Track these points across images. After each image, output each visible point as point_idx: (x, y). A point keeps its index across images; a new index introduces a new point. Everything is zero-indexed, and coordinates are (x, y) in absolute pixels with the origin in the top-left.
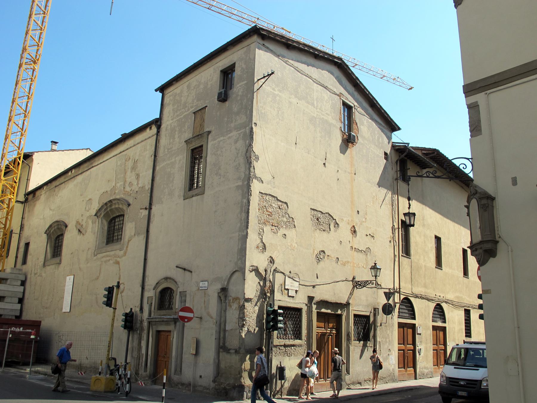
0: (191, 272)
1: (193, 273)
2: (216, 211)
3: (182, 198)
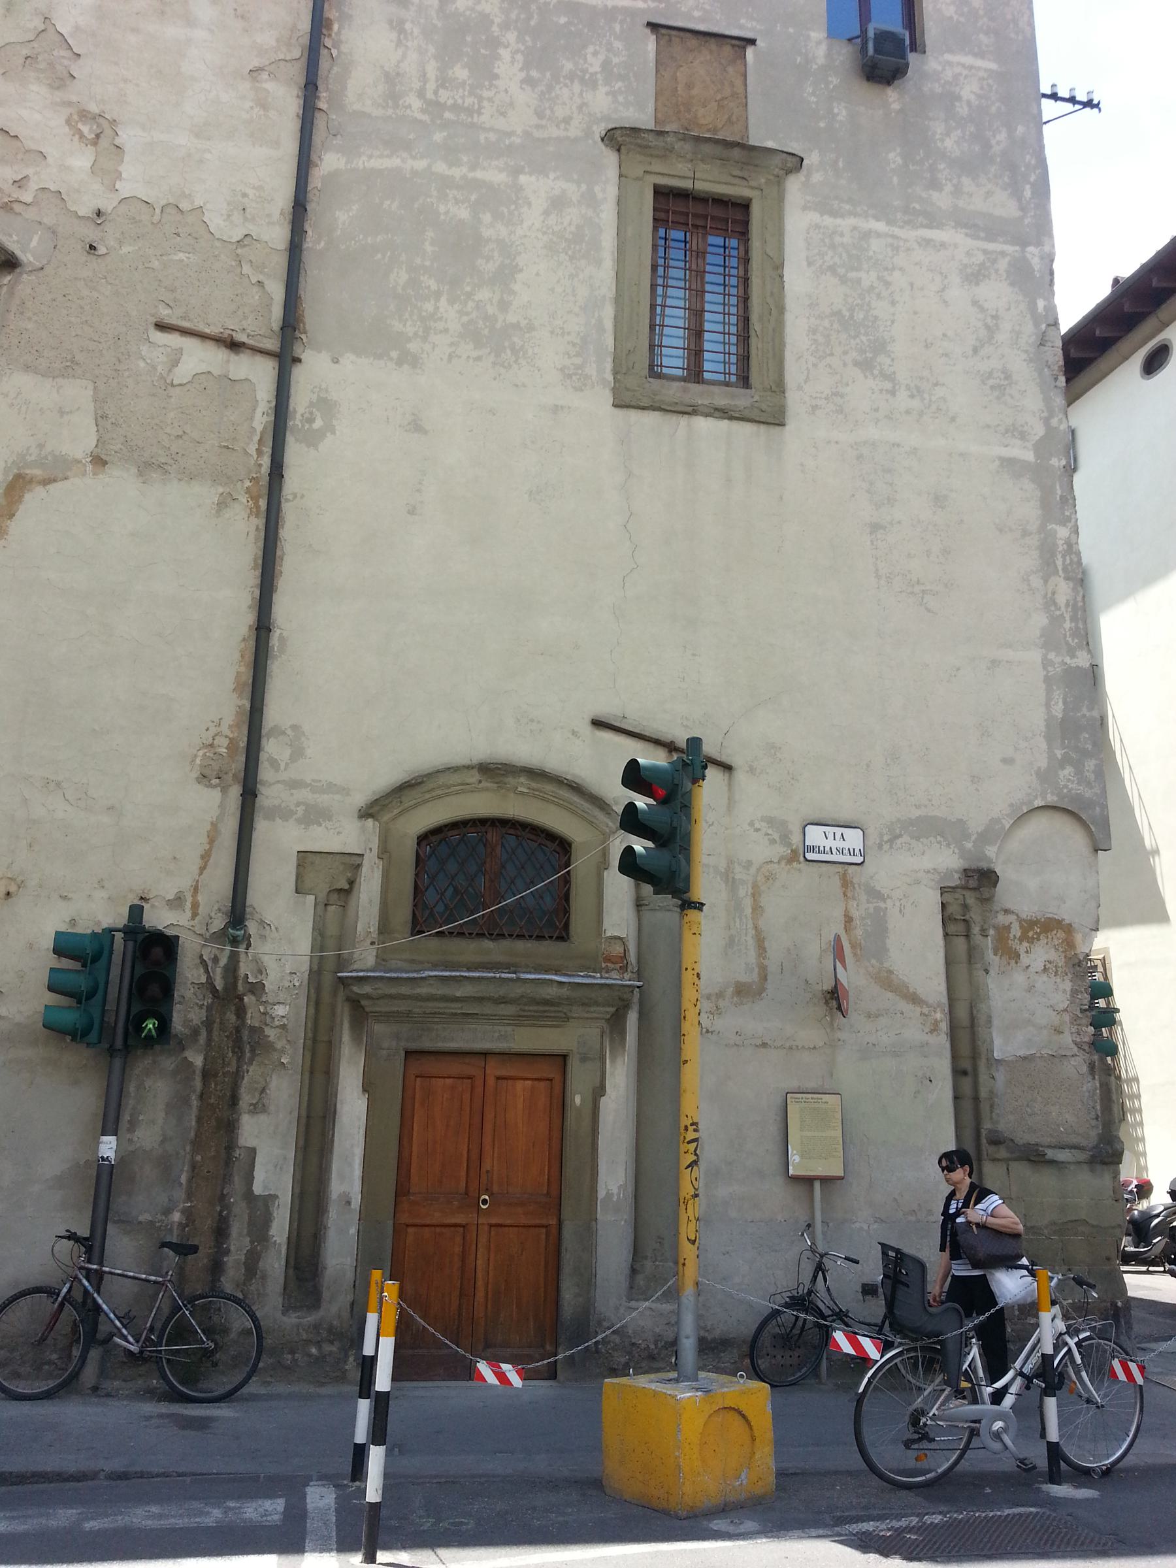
1: (740, 776)
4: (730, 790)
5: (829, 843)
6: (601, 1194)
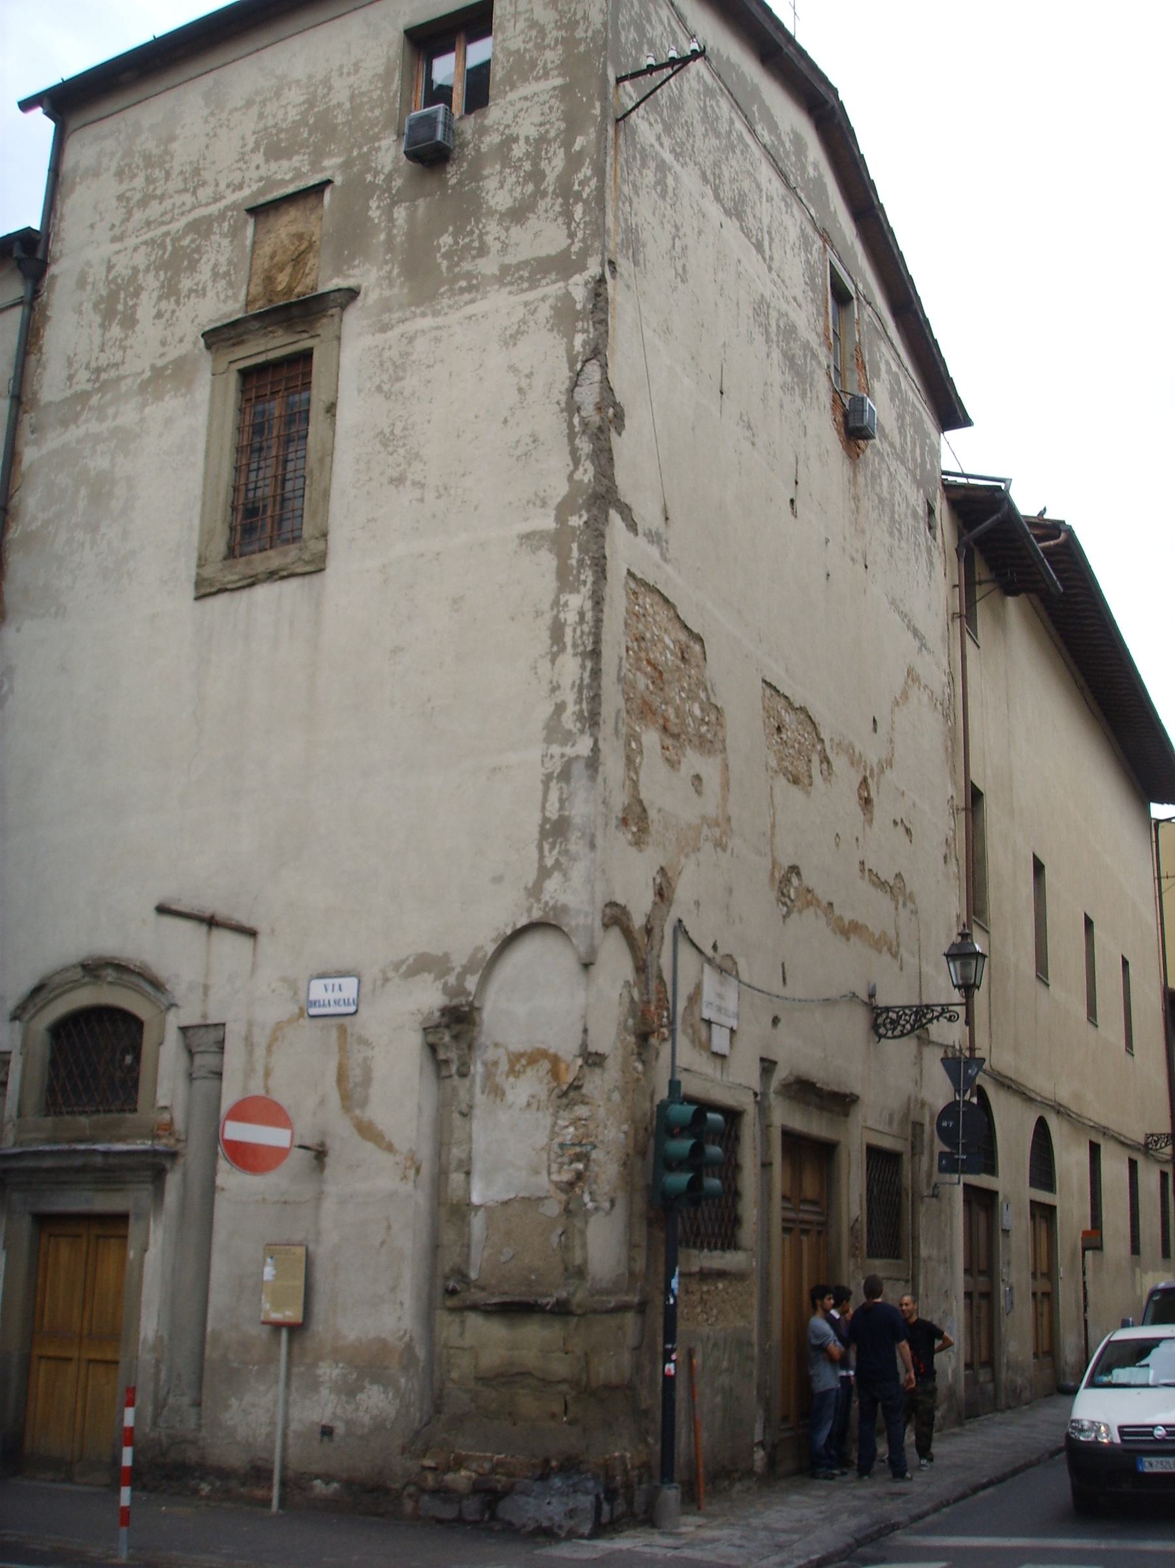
0: (252, 933)
1: (263, 939)
2: (396, 650)
3: (191, 592)
4: (254, 955)
5: (331, 996)
6: (142, 1337)
